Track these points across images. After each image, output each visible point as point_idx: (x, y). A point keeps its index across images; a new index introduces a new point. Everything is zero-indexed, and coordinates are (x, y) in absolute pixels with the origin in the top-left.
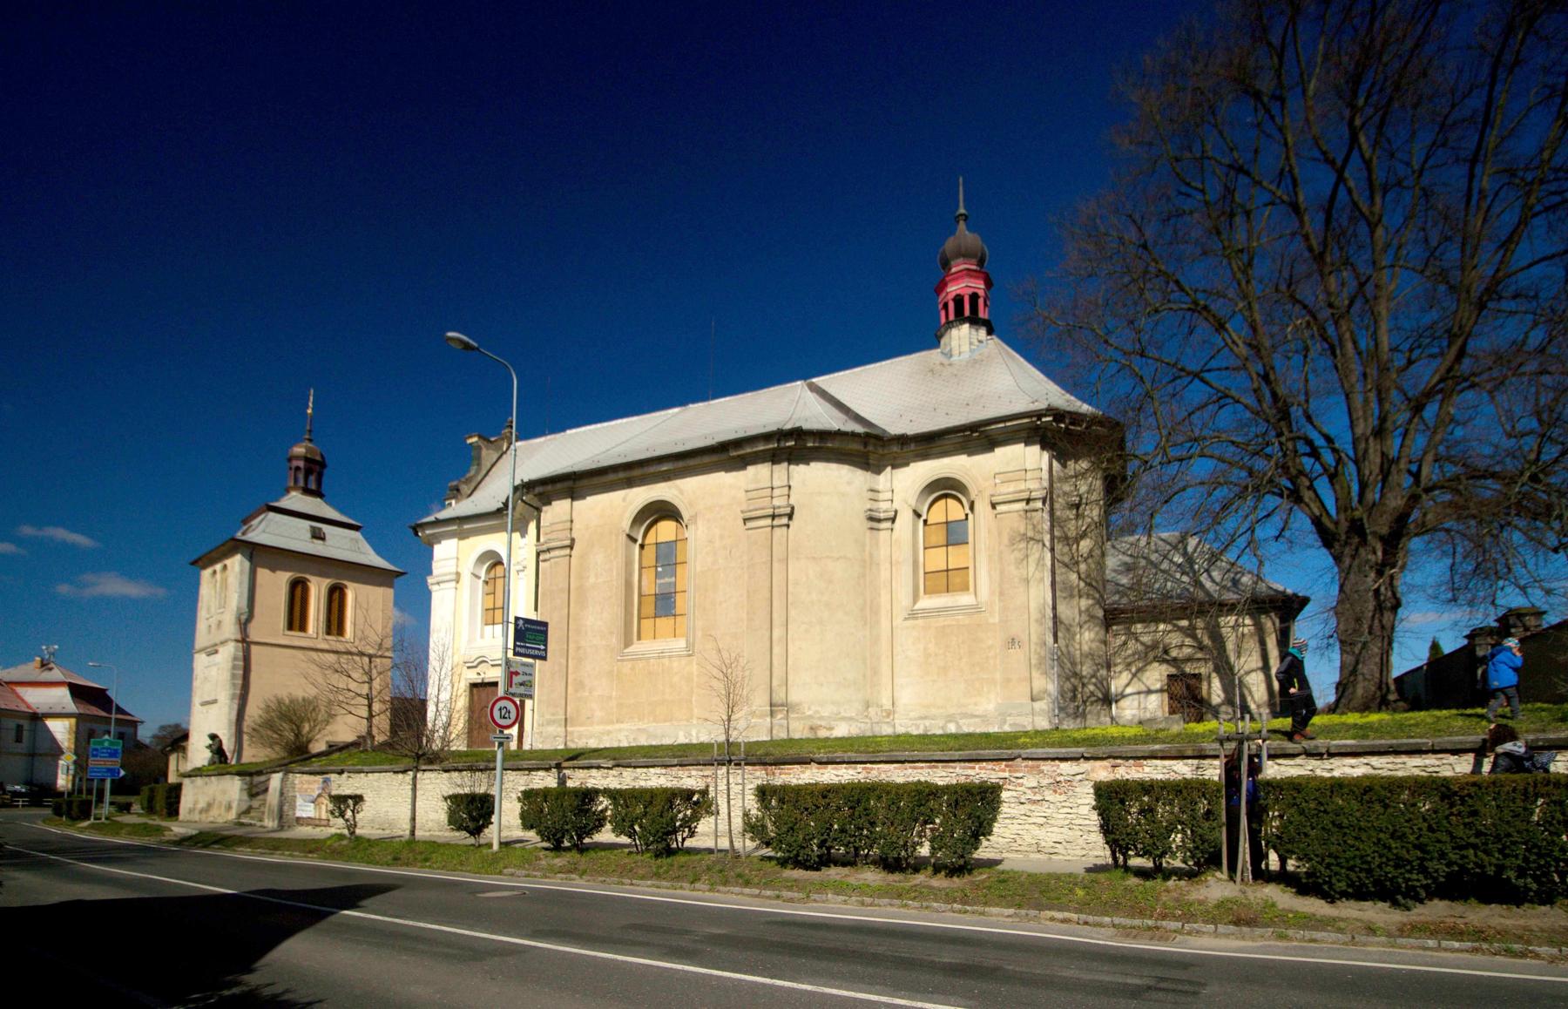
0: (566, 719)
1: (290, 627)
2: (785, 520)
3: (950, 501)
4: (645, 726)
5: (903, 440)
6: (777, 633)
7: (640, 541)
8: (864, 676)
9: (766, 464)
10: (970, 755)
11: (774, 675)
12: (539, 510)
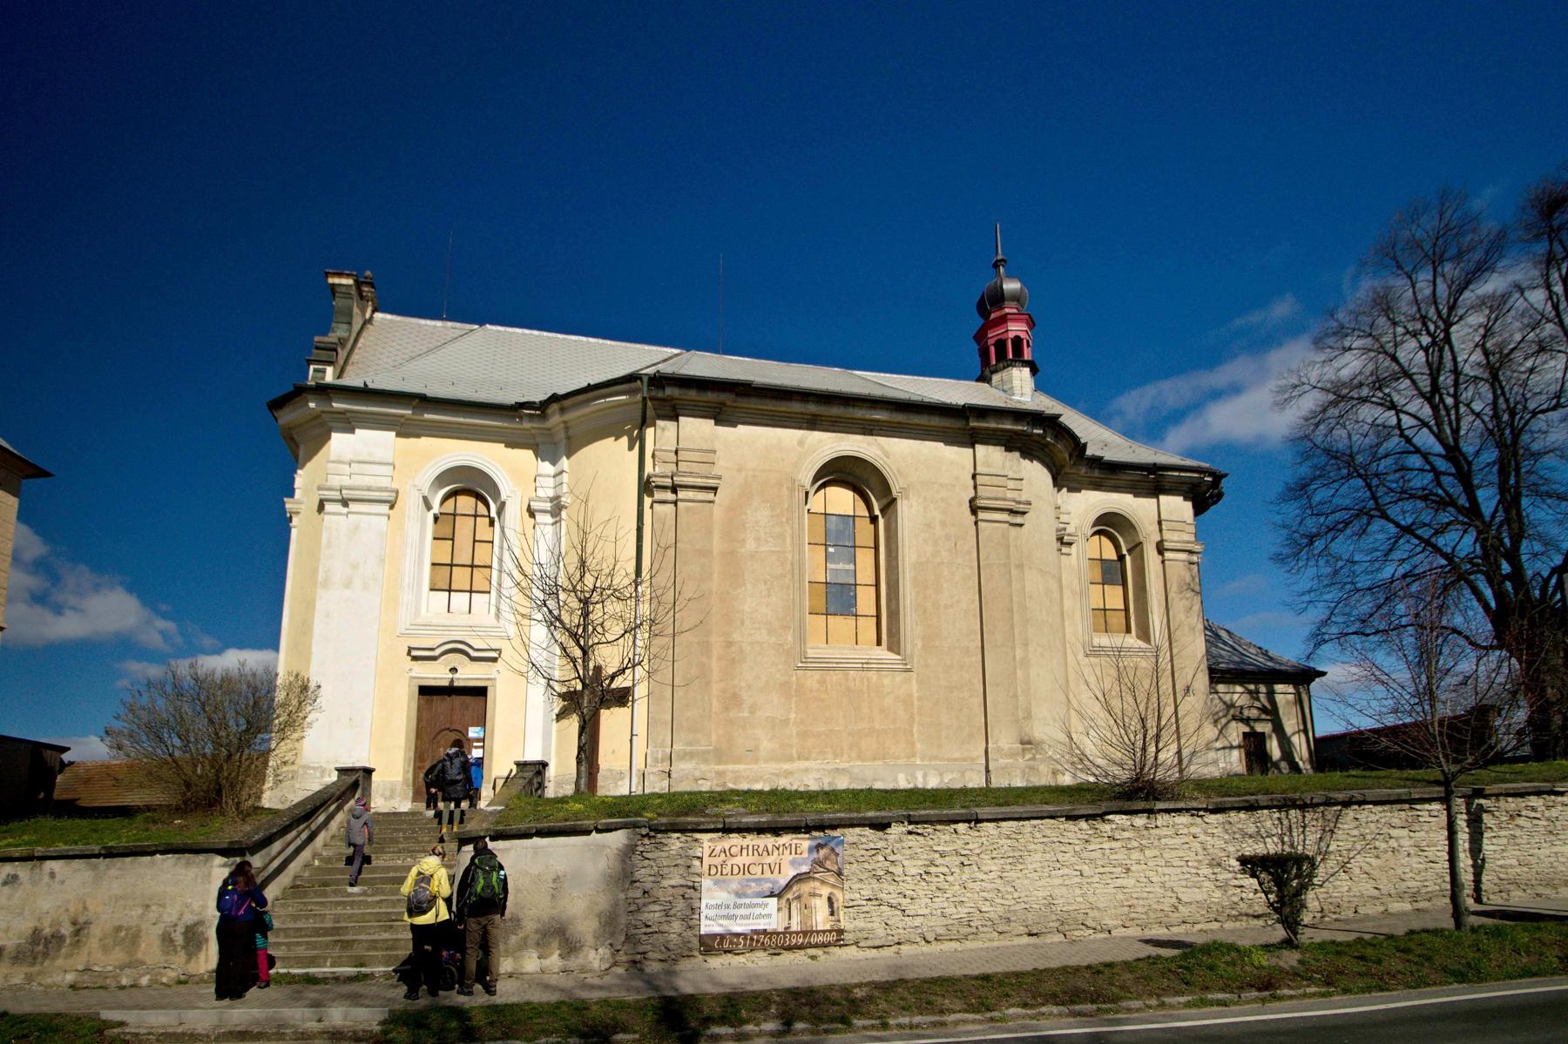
5: (1097, 462)
9: (998, 448)
10: (927, 815)
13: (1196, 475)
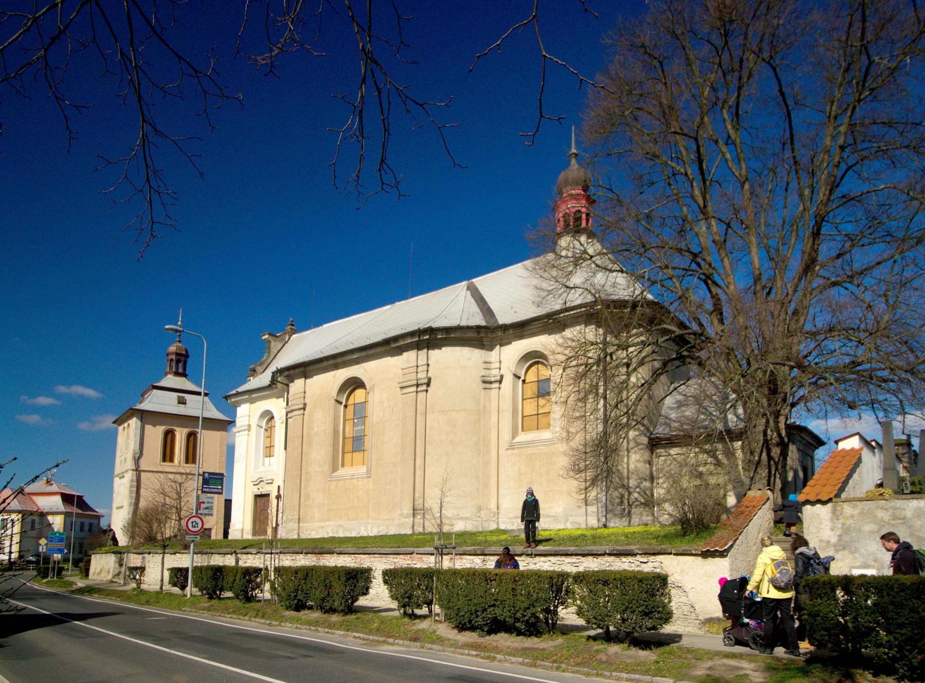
0: (299, 519)
1: (164, 460)
2: (424, 387)
3: (540, 366)
4: (342, 523)
6: (419, 462)
7: (344, 404)
8: (478, 489)
11: (416, 490)
12: (287, 385)
13: (583, 309)
